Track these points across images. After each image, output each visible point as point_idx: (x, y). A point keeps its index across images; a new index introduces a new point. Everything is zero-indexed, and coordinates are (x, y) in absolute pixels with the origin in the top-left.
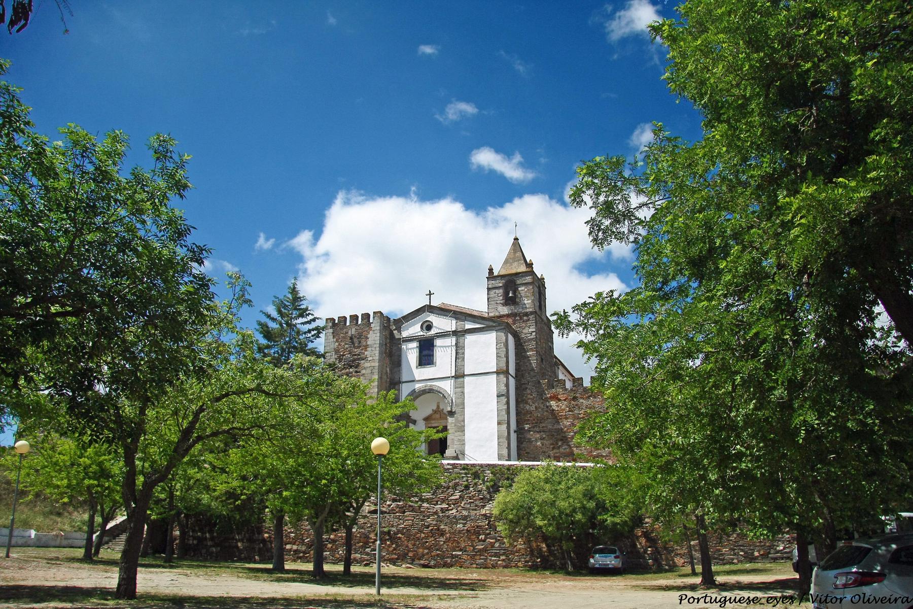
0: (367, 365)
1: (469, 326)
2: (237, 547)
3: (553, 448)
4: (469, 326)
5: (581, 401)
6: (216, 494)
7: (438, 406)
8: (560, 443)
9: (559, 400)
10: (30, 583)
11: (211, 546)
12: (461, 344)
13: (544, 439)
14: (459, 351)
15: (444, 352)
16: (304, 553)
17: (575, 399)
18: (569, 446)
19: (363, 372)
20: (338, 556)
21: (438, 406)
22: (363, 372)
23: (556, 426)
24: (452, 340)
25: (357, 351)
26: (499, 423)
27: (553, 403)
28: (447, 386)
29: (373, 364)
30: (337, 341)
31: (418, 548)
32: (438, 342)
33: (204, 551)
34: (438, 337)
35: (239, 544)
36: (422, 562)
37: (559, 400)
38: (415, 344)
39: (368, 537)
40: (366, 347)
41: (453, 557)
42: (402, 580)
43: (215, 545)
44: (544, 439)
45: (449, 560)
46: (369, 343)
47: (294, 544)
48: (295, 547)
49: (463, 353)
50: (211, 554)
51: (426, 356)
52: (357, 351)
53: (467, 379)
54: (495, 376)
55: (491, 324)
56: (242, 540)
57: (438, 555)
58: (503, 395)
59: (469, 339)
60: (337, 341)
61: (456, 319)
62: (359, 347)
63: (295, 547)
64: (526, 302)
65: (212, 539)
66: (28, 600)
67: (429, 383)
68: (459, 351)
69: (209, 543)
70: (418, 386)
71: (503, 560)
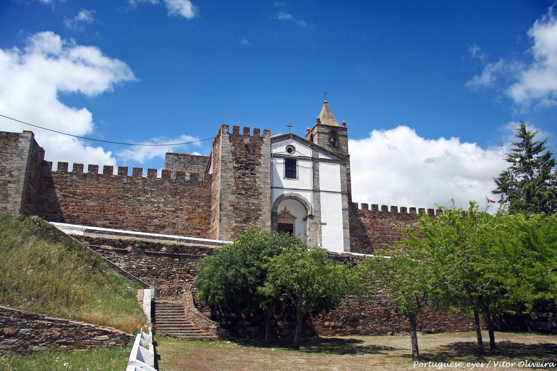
0: (261, 170)
1: (321, 156)
2: (277, 326)
3: (362, 248)
4: (321, 156)
5: (378, 219)
6: (534, 269)
7: (285, 209)
8: (366, 245)
9: (366, 217)
10: (346, 355)
11: (248, 326)
12: (316, 168)
13: (356, 241)
14: (315, 170)
15: (304, 170)
16: (341, 327)
17: (374, 218)
18: (372, 247)
19: (258, 175)
20: (368, 329)
21: (285, 209)
22: (258, 175)
23: (364, 234)
24: (309, 164)
25: (252, 157)
26: (344, 228)
27: (362, 218)
28: (308, 197)
29: (266, 171)
30: (234, 145)
31: (423, 320)
32: (300, 163)
33: (240, 331)
34: (300, 159)
35: (279, 323)
36: (427, 330)
37: (366, 217)
38: (282, 161)
39: (389, 313)
40: (260, 156)
41: (444, 325)
42: (368, 351)
43: (253, 325)
44: (356, 241)
45: (442, 327)
46: (261, 153)
47: (331, 321)
48: (333, 324)
49: (318, 175)
50: (249, 333)
51: (291, 172)
52: (252, 157)
53: (321, 194)
54: (340, 195)
55: (336, 158)
56: (281, 319)
57: (436, 324)
58: (346, 209)
59: (322, 166)
60: (234, 145)
61: (313, 149)
62: (253, 155)
63: (333, 324)
64: (343, 148)
65: (248, 318)
66: (473, 357)
67: (294, 192)
68: (315, 170)
69: (247, 323)
70: (286, 192)
71: (472, 326)
